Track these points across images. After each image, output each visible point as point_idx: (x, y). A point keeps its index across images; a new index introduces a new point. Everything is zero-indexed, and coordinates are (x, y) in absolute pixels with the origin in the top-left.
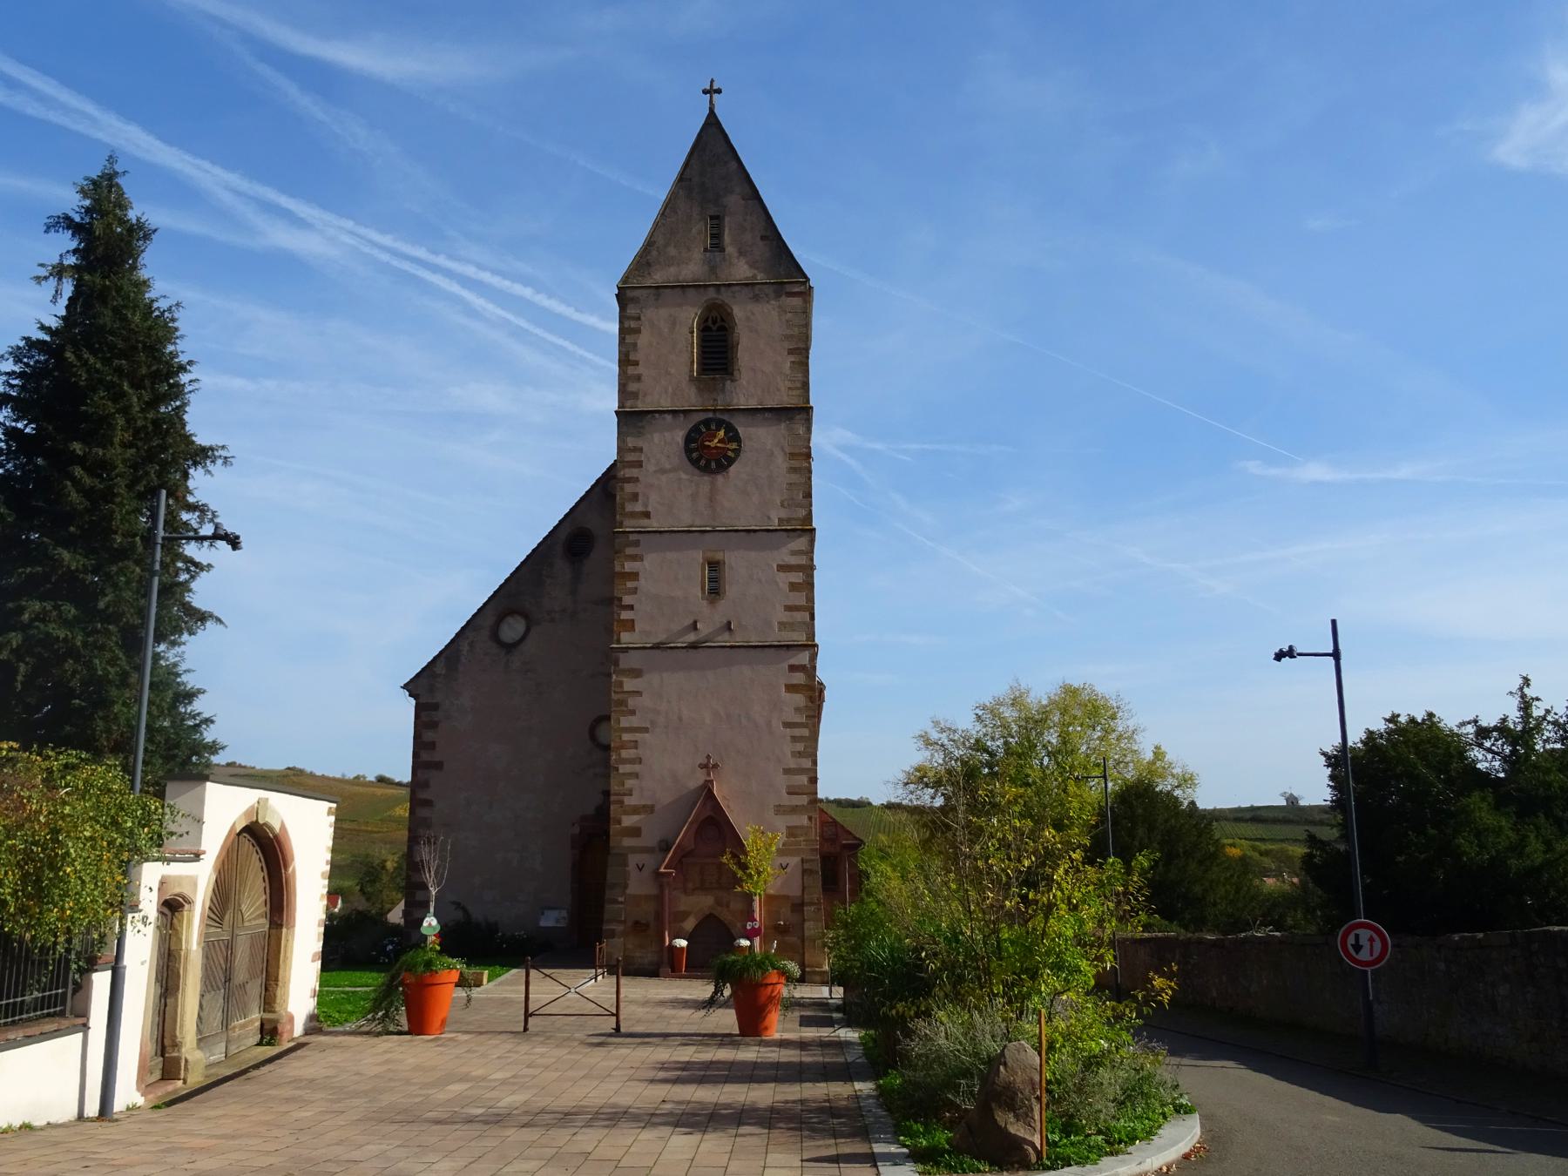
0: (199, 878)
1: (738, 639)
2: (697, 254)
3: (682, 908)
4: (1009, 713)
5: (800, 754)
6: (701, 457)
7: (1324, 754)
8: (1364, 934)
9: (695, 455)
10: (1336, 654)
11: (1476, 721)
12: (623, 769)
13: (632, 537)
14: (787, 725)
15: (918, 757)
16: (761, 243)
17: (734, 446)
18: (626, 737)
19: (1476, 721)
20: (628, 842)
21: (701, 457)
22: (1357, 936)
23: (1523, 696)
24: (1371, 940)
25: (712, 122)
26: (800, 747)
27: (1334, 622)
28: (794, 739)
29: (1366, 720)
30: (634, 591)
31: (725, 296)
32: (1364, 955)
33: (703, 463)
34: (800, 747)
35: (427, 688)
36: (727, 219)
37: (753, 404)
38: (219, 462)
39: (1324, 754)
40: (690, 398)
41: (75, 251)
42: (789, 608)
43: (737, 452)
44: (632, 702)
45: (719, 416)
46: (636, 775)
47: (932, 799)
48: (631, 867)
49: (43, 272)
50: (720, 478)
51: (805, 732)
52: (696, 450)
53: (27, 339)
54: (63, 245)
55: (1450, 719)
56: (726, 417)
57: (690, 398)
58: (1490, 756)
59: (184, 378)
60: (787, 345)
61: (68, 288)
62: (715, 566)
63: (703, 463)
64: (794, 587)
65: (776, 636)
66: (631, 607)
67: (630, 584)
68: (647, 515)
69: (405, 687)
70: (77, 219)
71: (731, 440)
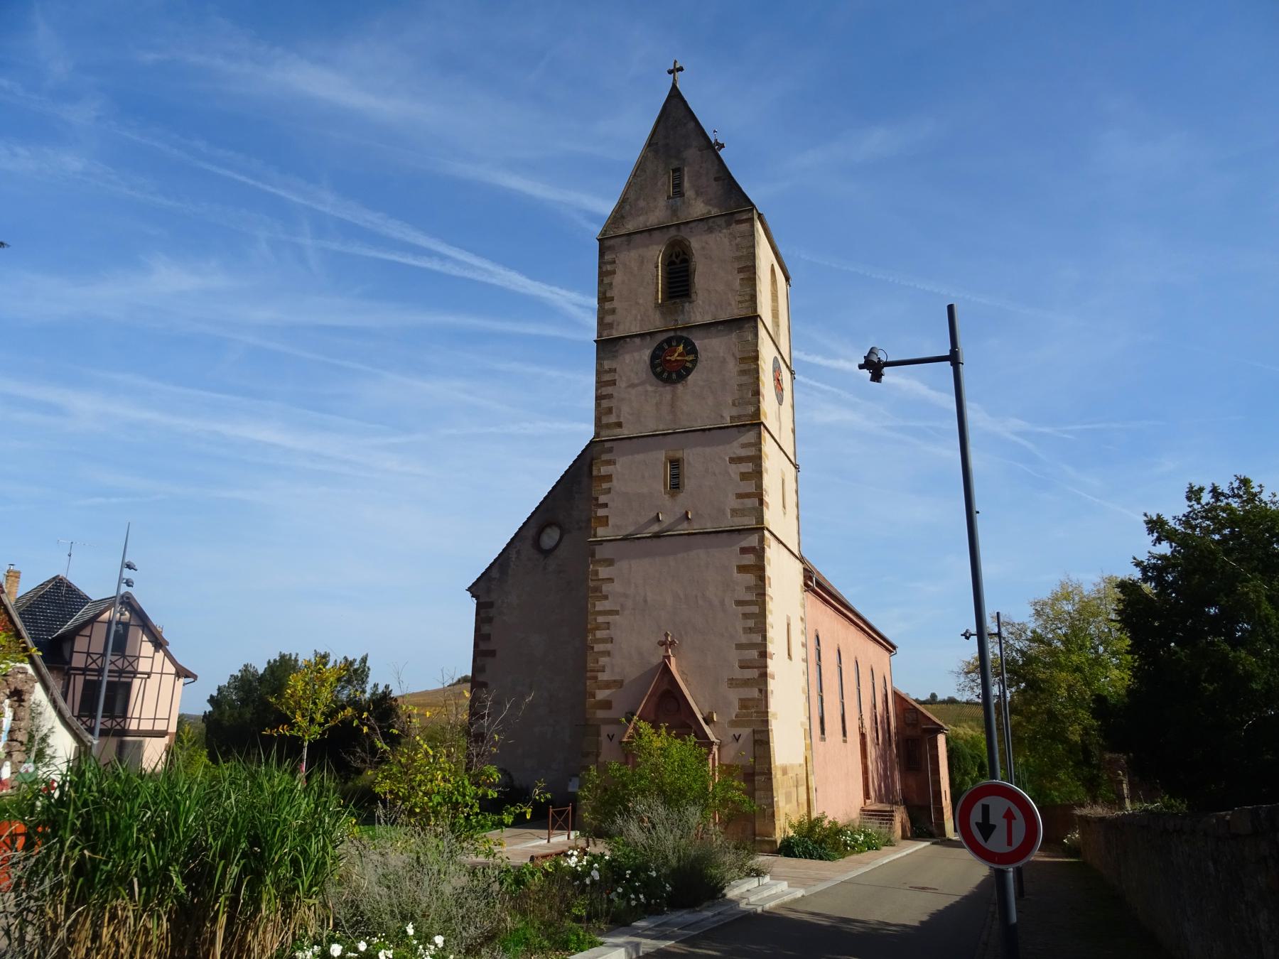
5: (750, 630)
6: (670, 374)
9: (658, 369)
10: (954, 358)
13: (607, 445)
14: (739, 603)
17: (691, 357)
18: (600, 619)
20: (601, 714)
21: (670, 374)
22: (986, 809)
24: (1009, 816)
26: (751, 623)
30: (609, 491)
33: (665, 375)
34: (751, 623)
35: (485, 590)
37: (708, 319)
40: (656, 321)
42: (740, 496)
43: (694, 362)
46: (608, 653)
48: (603, 738)
50: (680, 386)
51: (755, 609)
52: (660, 365)
56: (685, 334)
60: (737, 265)
62: (676, 464)
63: (665, 375)
64: (744, 476)
66: (606, 505)
67: (605, 486)
68: (619, 425)
69: (469, 589)
71: (688, 353)
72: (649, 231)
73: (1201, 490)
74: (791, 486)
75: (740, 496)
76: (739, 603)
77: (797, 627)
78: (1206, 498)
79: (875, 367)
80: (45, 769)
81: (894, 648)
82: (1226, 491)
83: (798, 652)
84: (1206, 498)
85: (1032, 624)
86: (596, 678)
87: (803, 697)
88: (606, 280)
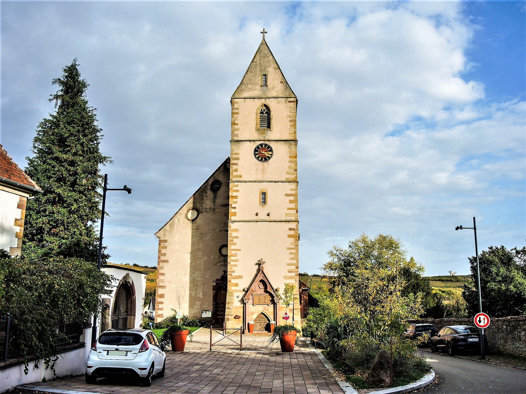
0: (111, 299)
1: (271, 218)
2: (258, 87)
3: (252, 311)
4: (361, 245)
5: (292, 259)
6: (259, 157)
7: (469, 259)
8: (482, 317)
10: (475, 229)
11: (515, 248)
12: (232, 263)
13: (236, 184)
14: (288, 249)
15: (328, 259)
16: (280, 84)
17: (270, 153)
18: (233, 252)
19: (515, 248)
20: (234, 288)
21: (259, 157)
24: (484, 319)
25: (264, 43)
26: (292, 256)
27: (474, 218)
28: (291, 254)
29: (484, 248)
30: (236, 203)
31: (269, 102)
32: (482, 324)
33: (260, 159)
34: (292, 256)
36: (269, 76)
38: (109, 162)
39: (469, 259)
40: (255, 136)
41: (62, 90)
42: (289, 209)
44: (235, 241)
45: (265, 142)
47: (334, 274)
48: (235, 297)
49: (52, 97)
50: (265, 164)
51: (294, 251)
53: (45, 119)
54: (58, 89)
55: (508, 249)
56: (268, 143)
57: (255, 136)
58: (520, 260)
59: (98, 134)
60: (289, 119)
61: (59, 102)
63: (260, 159)
64: (291, 202)
65: (284, 219)
66: (235, 208)
67: (235, 200)
68: (241, 176)
70: (62, 80)
75: (289, 209)
76: (288, 249)
80: (394, 330)
85: (348, 250)
86: (231, 275)
88: (235, 116)
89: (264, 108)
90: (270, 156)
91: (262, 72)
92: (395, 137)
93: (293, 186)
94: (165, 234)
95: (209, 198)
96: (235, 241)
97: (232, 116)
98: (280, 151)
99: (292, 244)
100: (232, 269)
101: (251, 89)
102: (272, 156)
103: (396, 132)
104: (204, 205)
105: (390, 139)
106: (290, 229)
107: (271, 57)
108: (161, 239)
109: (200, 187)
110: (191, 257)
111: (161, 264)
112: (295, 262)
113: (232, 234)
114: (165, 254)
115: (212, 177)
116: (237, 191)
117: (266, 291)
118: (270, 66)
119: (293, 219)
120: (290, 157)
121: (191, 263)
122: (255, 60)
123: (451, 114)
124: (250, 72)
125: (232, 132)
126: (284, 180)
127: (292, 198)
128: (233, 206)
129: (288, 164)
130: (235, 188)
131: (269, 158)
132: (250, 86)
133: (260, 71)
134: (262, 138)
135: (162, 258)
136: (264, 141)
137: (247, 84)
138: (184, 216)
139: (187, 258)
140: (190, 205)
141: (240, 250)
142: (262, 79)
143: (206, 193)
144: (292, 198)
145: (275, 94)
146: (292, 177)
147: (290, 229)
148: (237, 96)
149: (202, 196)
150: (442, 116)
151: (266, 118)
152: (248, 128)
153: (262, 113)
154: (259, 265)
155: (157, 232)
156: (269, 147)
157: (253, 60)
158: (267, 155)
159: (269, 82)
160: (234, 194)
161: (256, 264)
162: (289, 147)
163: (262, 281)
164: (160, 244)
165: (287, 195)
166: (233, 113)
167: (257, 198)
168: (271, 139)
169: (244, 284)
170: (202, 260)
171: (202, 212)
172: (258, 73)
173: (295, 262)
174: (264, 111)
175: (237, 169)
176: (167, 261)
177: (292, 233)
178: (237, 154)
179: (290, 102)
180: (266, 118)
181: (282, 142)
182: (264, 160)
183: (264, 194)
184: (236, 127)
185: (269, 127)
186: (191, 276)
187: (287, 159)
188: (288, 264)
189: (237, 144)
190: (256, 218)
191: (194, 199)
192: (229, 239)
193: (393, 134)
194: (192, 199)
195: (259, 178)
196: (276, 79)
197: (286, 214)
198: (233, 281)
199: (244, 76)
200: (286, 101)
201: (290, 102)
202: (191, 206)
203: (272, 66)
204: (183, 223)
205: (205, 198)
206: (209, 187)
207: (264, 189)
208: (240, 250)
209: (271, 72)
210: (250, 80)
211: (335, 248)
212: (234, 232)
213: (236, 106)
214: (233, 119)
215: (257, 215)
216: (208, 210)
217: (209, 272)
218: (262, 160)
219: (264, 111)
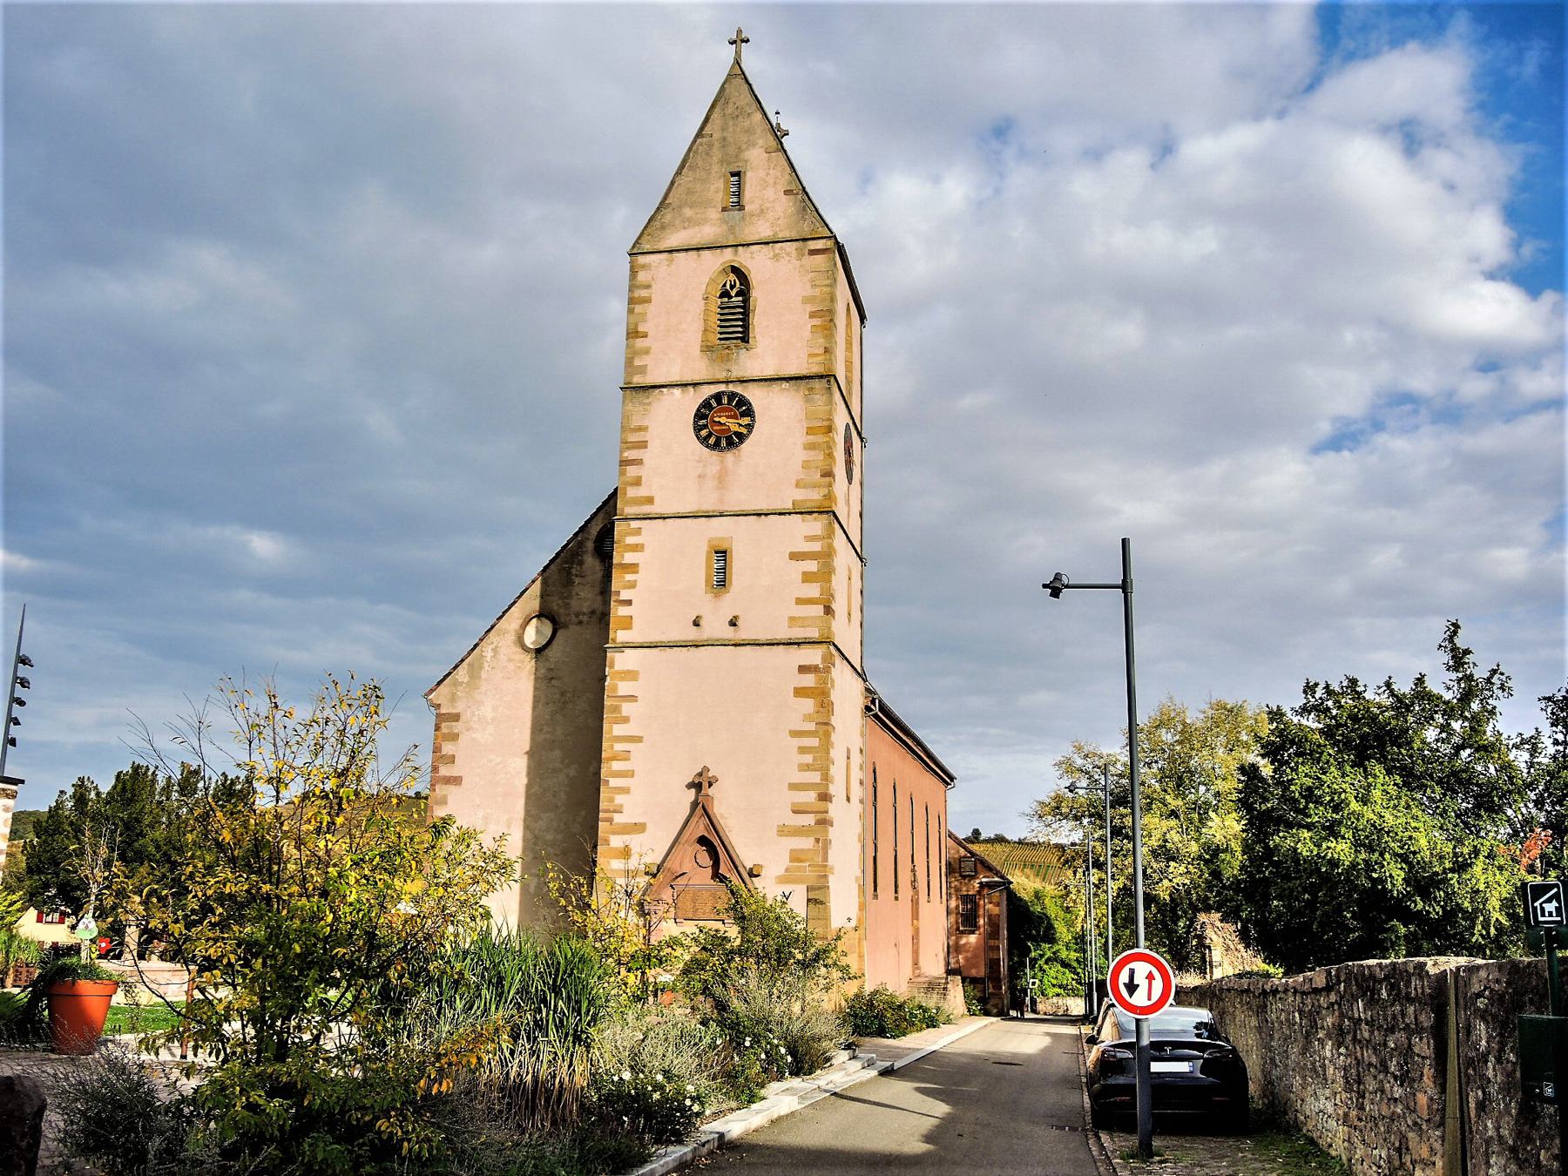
1: (744, 633)
2: (714, 214)
6: (710, 435)
8: (1142, 969)
10: (1125, 587)
12: (614, 782)
13: (634, 524)
14: (796, 734)
16: (784, 198)
17: (746, 421)
18: (619, 747)
21: (710, 435)
22: (1132, 972)
23: (1454, 649)
24: (1150, 977)
25: (738, 72)
26: (808, 759)
28: (803, 750)
30: (632, 585)
31: (744, 259)
33: (712, 440)
34: (808, 759)
36: (749, 174)
40: (699, 368)
44: (626, 709)
45: (731, 388)
46: (626, 791)
50: (729, 456)
51: (813, 742)
56: (738, 389)
60: (809, 308)
63: (712, 440)
64: (807, 577)
65: (784, 633)
66: (629, 603)
67: (629, 577)
68: (650, 500)
72: (698, 249)
73: (1316, 685)
74: (857, 584)
76: (796, 734)
77: (856, 759)
78: (1320, 692)
79: (1055, 588)
81: (952, 779)
82: (1337, 689)
83: (857, 792)
84: (1320, 692)
86: (610, 820)
87: (859, 846)
88: (638, 309)
89: (732, 277)
90: (744, 431)
91: (729, 164)
92: (1346, 454)
93: (816, 525)
94: (454, 694)
95: (589, 579)
96: (626, 709)
97: (631, 311)
98: (778, 414)
99: (807, 718)
100: (611, 800)
101: (691, 223)
102: (750, 432)
103: (1344, 438)
104: (574, 603)
105: (1331, 457)
106: (803, 669)
107: (759, 116)
108: (443, 711)
109: (564, 548)
110: (529, 767)
111: (441, 790)
112: (815, 777)
113: (616, 686)
114: (451, 759)
115: (601, 515)
116: (637, 548)
117: (716, 875)
118: (754, 145)
119: (814, 634)
120: (810, 431)
121: (529, 787)
122: (707, 130)
123: (1503, 381)
124: (691, 168)
125: (629, 362)
126: (789, 506)
127: (812, 566)
128: (624, 595)
129: (801, 455)
130: (630, 540)
131: (742, 437)
132: (688, 212)
133: (721, 162)
134: (722, 376)
135: (444, 771)
136: (727, 382)
137: (680, 207)
138: (511, 637)
139: (516, 771)
140: (532, 602)
141: (639, 739)
142: (726, 189)
143: (581, 563)
144: (812, 566)
145: (765, 232)
146: (814, 496)
147: (803, 669)
148: (647, 247)
149: (569, 573)
150: (1476, 388)
151: (735, 311)
152: (680, 349)
153: (725, 294)
154: (697, 786)
155: (432, 691)
156: (743, 402)
157: (702, 128)
158: (735, 428)
159: (748, 194)
160: (629, 558)
161: (690, 786)
162: (807, 399)
163: (703, 841)
164: (437, 728)
165: (795, 556)
166: (631, 301)
167: (698, 569)
168: (748, 374)
169: (650, 848)
170: (562, 777)
171: (565, 626)
172: (716, 168)
173: (815, 777)
174: (732, 287)
175: (639, 478)
176: (456, 781)
177: (809, 680)
178: (640, 429)
179: (813, 252)
180: (735, 311)
181: (785, 385)
182: (724, 443)
183: (723, 554)
184: (640, 343)
185: (745, 338)
186: (527, 828)
187: (800, 437)
188: (794, 787)
189: (641, 396)
190: (692, 634)
191: (544, 583)
192: (607, 702)
193: (1336, 443)
194: (538, 583)
195: (709, 505)
196: (771, 182)
197: (792, 619)
198: (616, 841)
199: (672, 183)
200: (800, 255)
201: (813, 252)
202: (535, 605)
203: (761, 142)
204: (510, 660)
205: (577, 580)
206: (590, 545)
207: (721, 539)
208: (639, 739)
209: (757, 160)
210: (690, 192)
211: (1079, 749)
212: (623, 679)
213: (642, 277)
214: (632, 320)
215: (696, 624)
216: (585, 618)
217: (583, 813)
218: (716, 446)
219: (732, 287)
